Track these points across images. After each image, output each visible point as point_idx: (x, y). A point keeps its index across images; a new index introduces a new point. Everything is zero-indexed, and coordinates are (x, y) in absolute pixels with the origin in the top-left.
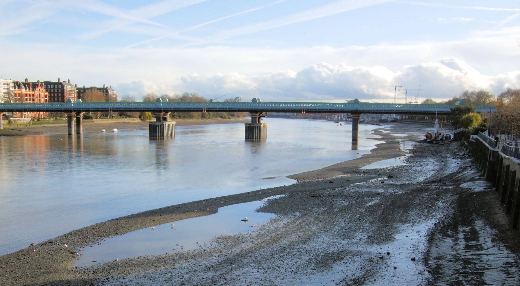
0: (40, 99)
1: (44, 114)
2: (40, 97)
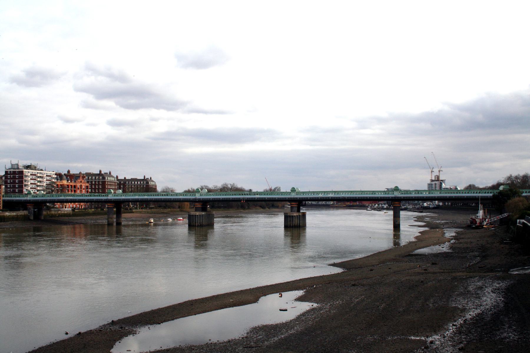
0: (81, 190)
1: (85, 205)
2: (81, 188)
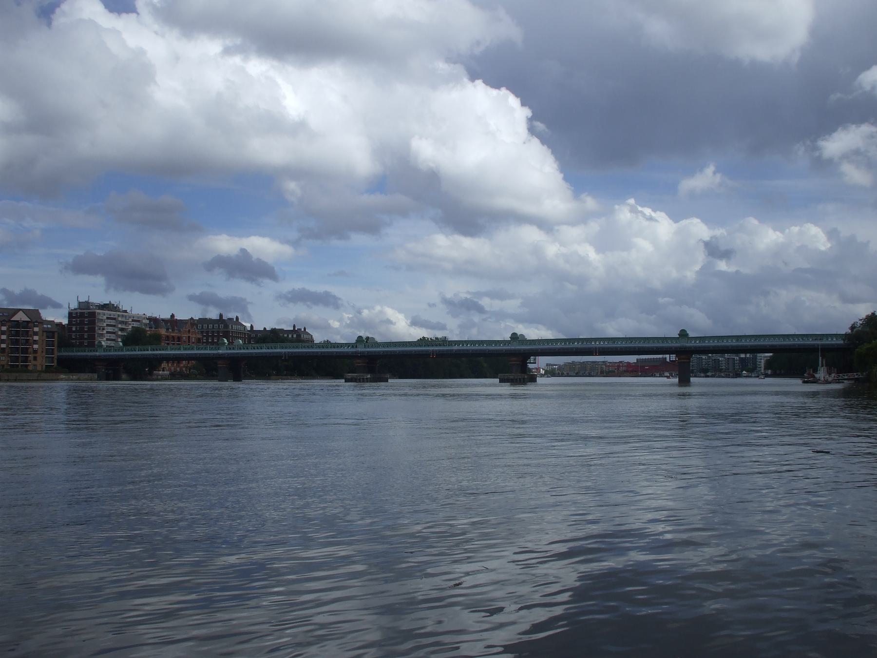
2: (189, 342)
